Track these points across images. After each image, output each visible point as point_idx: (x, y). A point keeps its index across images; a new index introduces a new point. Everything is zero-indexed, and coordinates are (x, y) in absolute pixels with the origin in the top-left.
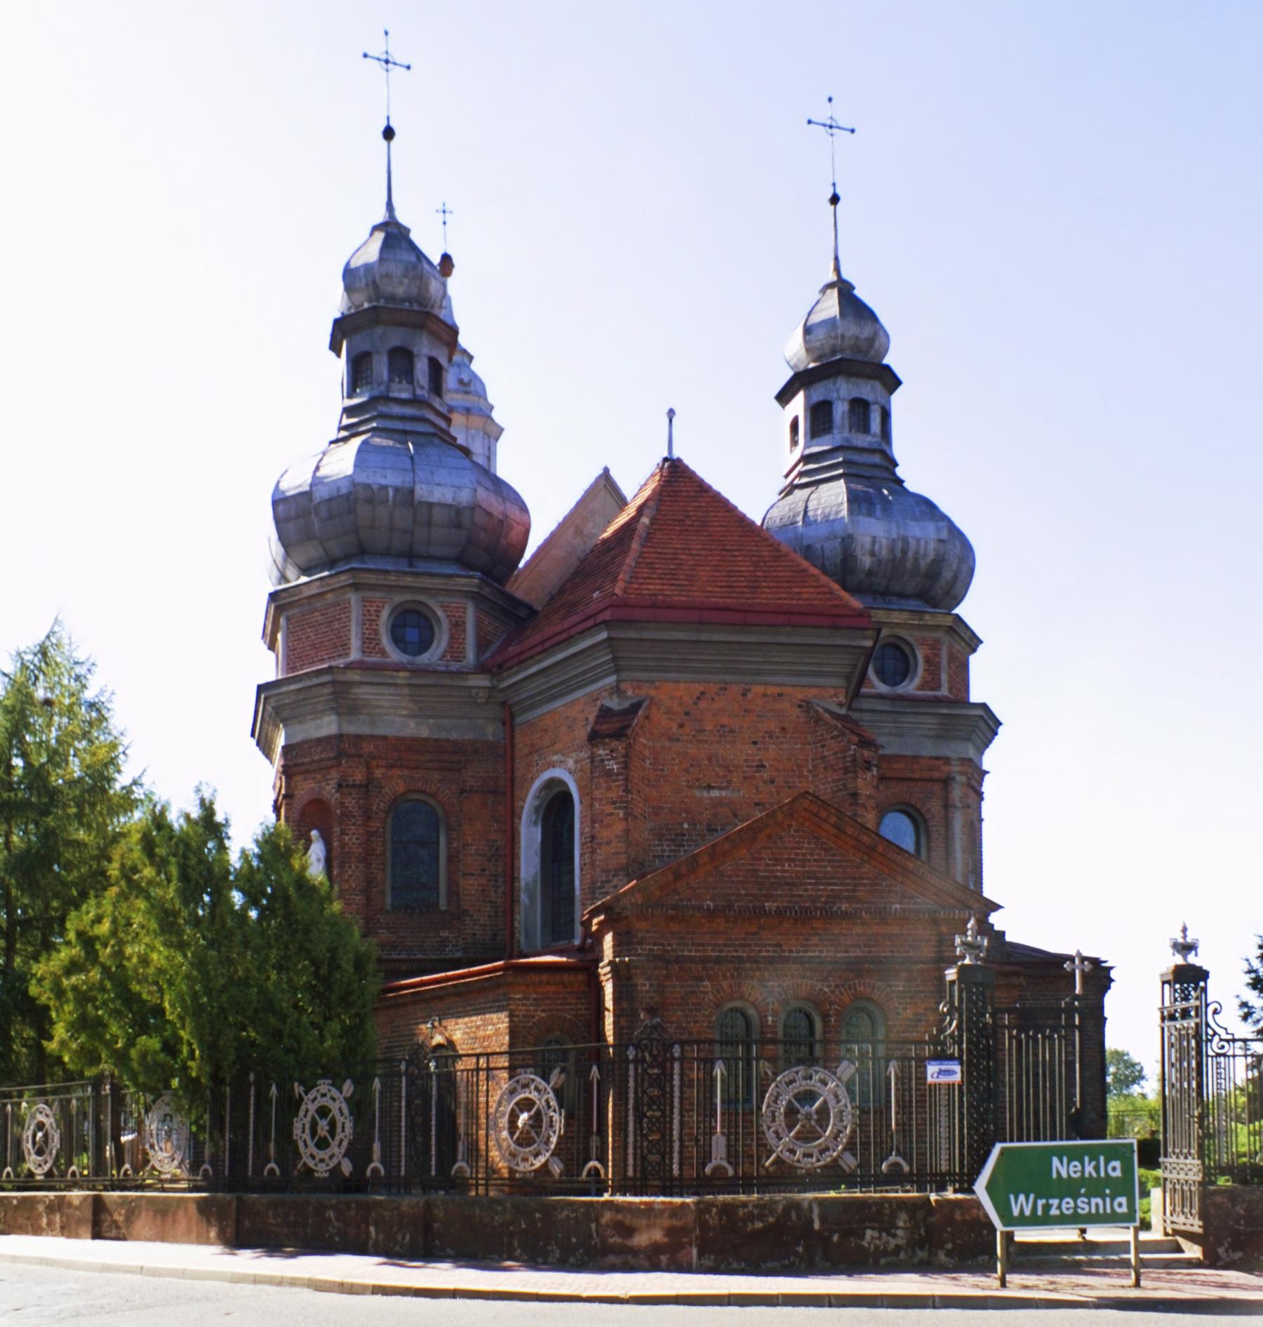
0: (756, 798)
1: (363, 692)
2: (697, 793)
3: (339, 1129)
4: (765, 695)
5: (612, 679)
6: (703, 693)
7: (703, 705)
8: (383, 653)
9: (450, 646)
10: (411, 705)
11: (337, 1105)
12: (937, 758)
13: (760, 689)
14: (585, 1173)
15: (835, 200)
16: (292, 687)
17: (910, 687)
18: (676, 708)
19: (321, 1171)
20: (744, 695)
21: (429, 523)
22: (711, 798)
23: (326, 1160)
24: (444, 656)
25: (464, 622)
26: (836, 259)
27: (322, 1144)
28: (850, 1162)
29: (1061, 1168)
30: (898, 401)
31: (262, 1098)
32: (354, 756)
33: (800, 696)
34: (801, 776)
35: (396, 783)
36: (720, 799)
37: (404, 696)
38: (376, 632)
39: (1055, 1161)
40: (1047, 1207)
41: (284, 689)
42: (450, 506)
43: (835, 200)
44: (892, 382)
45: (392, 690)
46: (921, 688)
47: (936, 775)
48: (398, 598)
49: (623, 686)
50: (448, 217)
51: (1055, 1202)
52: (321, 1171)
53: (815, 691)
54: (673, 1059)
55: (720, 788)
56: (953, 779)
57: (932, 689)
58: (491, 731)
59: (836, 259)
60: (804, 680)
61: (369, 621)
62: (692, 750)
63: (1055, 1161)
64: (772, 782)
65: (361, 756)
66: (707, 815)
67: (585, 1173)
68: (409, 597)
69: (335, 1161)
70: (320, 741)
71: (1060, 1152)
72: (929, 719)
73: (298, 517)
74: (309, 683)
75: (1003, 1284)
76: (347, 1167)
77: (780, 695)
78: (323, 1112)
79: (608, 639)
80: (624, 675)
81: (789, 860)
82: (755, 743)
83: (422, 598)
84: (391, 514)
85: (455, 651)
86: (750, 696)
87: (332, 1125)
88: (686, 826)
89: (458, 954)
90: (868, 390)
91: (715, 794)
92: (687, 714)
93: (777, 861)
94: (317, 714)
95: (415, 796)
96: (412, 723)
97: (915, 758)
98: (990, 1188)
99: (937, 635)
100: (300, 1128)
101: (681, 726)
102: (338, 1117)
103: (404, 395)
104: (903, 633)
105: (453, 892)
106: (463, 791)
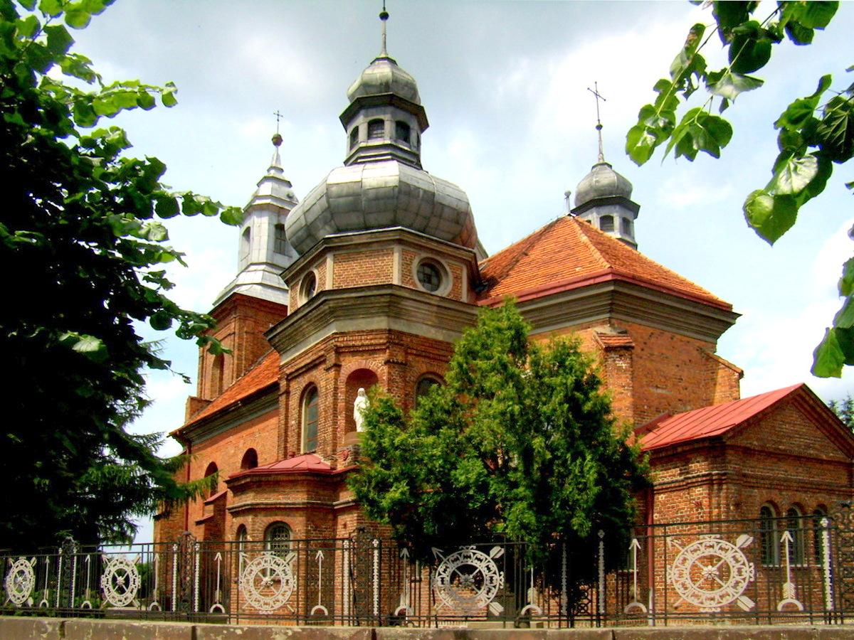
0: (679, 397)
1: (409, 305)
3: (131, 583)
5: (608, 315)
6: (652, 334)
7: (653, 340)
8: (415, 285)
9: (453, 290)
10: (434, 319)
11: (689, 556)
14: (82, 606)
16: (353, 295)
19: (18, 603)
20: (672, 339)
21: (440, 217)
22: (658, 394)
25: (461, 278)
28: (747, 604)
32: (397, 344)
33: (698, 344)
34: (699, 388)
36: (662, 395)
37: (432, 312)
38: (410, 271)
41: (345, 296)
42: (455, 209)
45: (426, 307)
48: (424, 255)
49: (613, 321)
53: (703, 343)
54: (373, 548)
55: (663, 389)
59: (601, 153)
60: (699, 337)
61: (405, 266)
65: (402, 345)
66: (656, 403)
67: (82, 606)
68: (430, 255)
69: (25, 599)
73: (348, 195)
74: (369, 293)
76: (31, 602)
77: (688, 342)
79: (613, 291)
80: (614, 315)
81: (788, 423)
82: (678, 366)
83: (438, 258)
86: (675, 339)
87: (127, 580)
88: (646, 407)
90: (629, 215)
91: (660, 391)
92: (645, 343)
95: (430, 376)
96: (433, 330)
100: (105, 581)
101: (642, 350)
102: (131, 576)
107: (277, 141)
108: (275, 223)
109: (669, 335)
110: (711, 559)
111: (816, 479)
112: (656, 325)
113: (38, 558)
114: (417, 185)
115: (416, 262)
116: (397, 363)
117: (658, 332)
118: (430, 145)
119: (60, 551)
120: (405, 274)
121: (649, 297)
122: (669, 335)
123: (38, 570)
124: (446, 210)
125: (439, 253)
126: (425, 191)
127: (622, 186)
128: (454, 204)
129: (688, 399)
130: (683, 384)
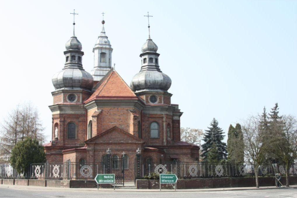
1: (63, 108)
2: (110, 123)
4: (121, 109)
6: (111, 109)
7: (111, 110)
12: (161, 114)
13: (120, 108)
15: (149, 27)
17: (156, 103)
18: (107, 111)
19: (56, 177)
21: (75, 82)
23: (56, 175)
24: (76, 102)
26: (149, 36)
27: (56, 173)
28: (223, 175)
29: (105, 177)
30: (160, 58)
31: (49, 167)
35: (69, 120)
38: (66, 98)
39: (104, 176)
40: (103, 181)
42: (78, 80)
43: (149, 27)
44: (158, 55)
46: (159, 103)
47: (160, 117)
48: (69, 94)
50: (104, 14)
51: (104, 181)
52: (56, 177)
53: (129, 108)
56: (163, 117)
57: (160, 103)
58: (84, 112)
59: (149, 36)
61: (64, 97)
62: (109, 117)
63: (104, 176)
64: (122, 121)
65: (63, 117)
68: (71, 93)
70: (57, 114)
71: (105, 175)
72: (158, 108)
73: (55, 81)
75: (114, 190)
78: (56, 169)
80: (99, 107)
82: (119, 116)
84: (69, 81)
85: (78, 101)
86: (118, 109)
89: (78, 146)
91: (113, 123)
93: (112, 135)
94: (57, 111)
97: (156, 114)
98: (97, 179)
99: (161, 95)
100: (53, 172)
101: (107, 114)
103: (74, 62)
104: (155, 95)
105: (78, 136)
106: (79, 121)
107: (103, 22)
108: (100, 52)
109: (117, 108)
110: (161, 168)
111: (123, 148)
112: (112, 106)
113: (60, 165)
114: (67, 77)
115: (67, 96)
116: (62, 121)
117: (112, 108)
118: (108, 39)
119: (45, 164)
120: (65, 100)
121: (88, 104)
122: (117, 108)
123: (41, 168)
124: (76, 81)
125: (73, 92)
126: (70, 78)
127: (86, 79)
128: (78, 79)
129: (123, 124)
130: (121, 120)
